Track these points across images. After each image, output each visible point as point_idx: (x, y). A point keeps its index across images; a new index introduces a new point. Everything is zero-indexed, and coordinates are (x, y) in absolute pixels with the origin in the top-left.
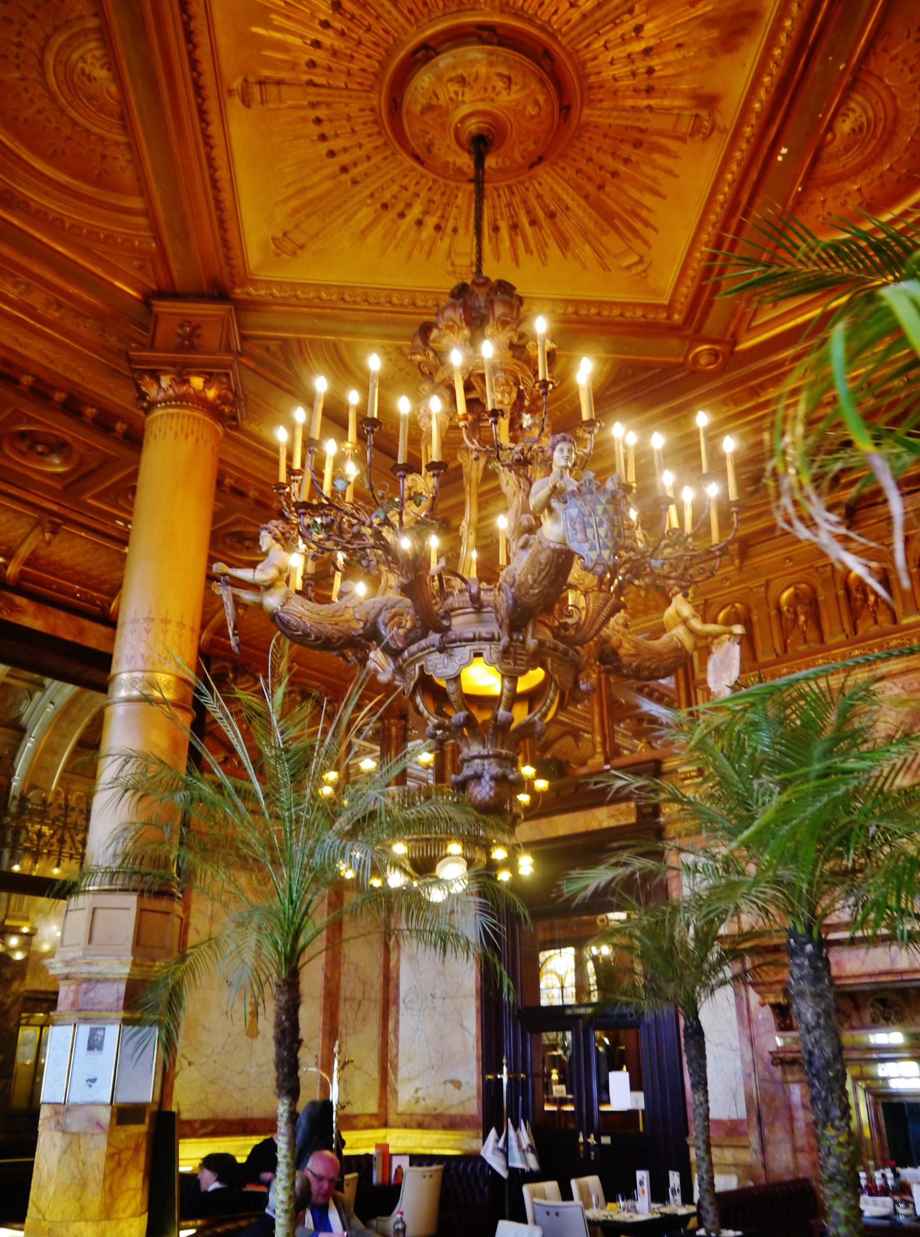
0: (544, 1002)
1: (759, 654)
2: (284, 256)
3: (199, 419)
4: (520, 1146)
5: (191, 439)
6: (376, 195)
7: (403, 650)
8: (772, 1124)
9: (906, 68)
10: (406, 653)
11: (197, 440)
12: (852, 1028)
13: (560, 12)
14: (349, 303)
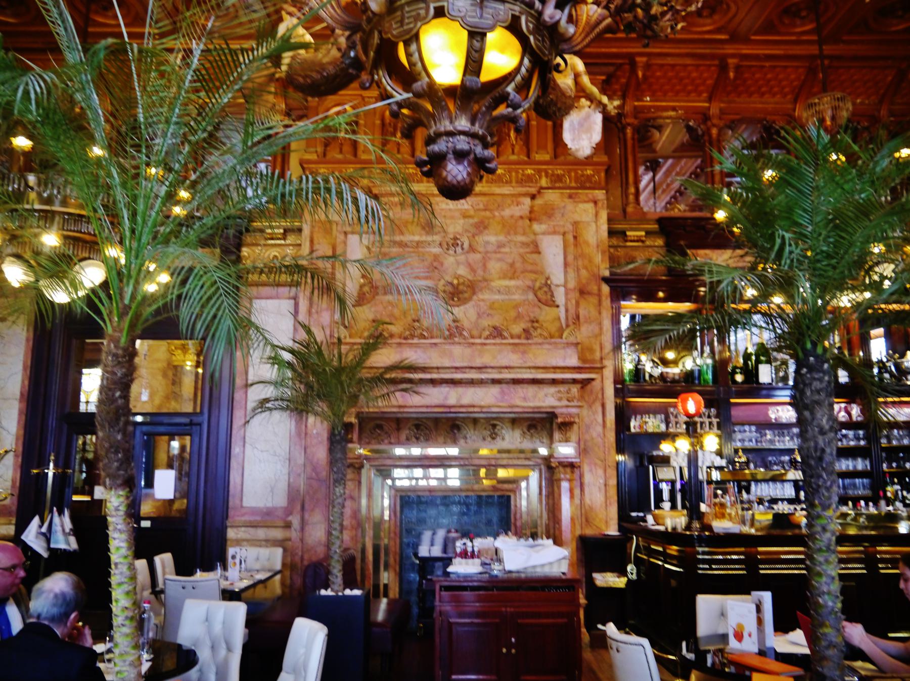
0: (83, 408)
4: (64, 530)
8: (312, 510)
12: (390, 443)
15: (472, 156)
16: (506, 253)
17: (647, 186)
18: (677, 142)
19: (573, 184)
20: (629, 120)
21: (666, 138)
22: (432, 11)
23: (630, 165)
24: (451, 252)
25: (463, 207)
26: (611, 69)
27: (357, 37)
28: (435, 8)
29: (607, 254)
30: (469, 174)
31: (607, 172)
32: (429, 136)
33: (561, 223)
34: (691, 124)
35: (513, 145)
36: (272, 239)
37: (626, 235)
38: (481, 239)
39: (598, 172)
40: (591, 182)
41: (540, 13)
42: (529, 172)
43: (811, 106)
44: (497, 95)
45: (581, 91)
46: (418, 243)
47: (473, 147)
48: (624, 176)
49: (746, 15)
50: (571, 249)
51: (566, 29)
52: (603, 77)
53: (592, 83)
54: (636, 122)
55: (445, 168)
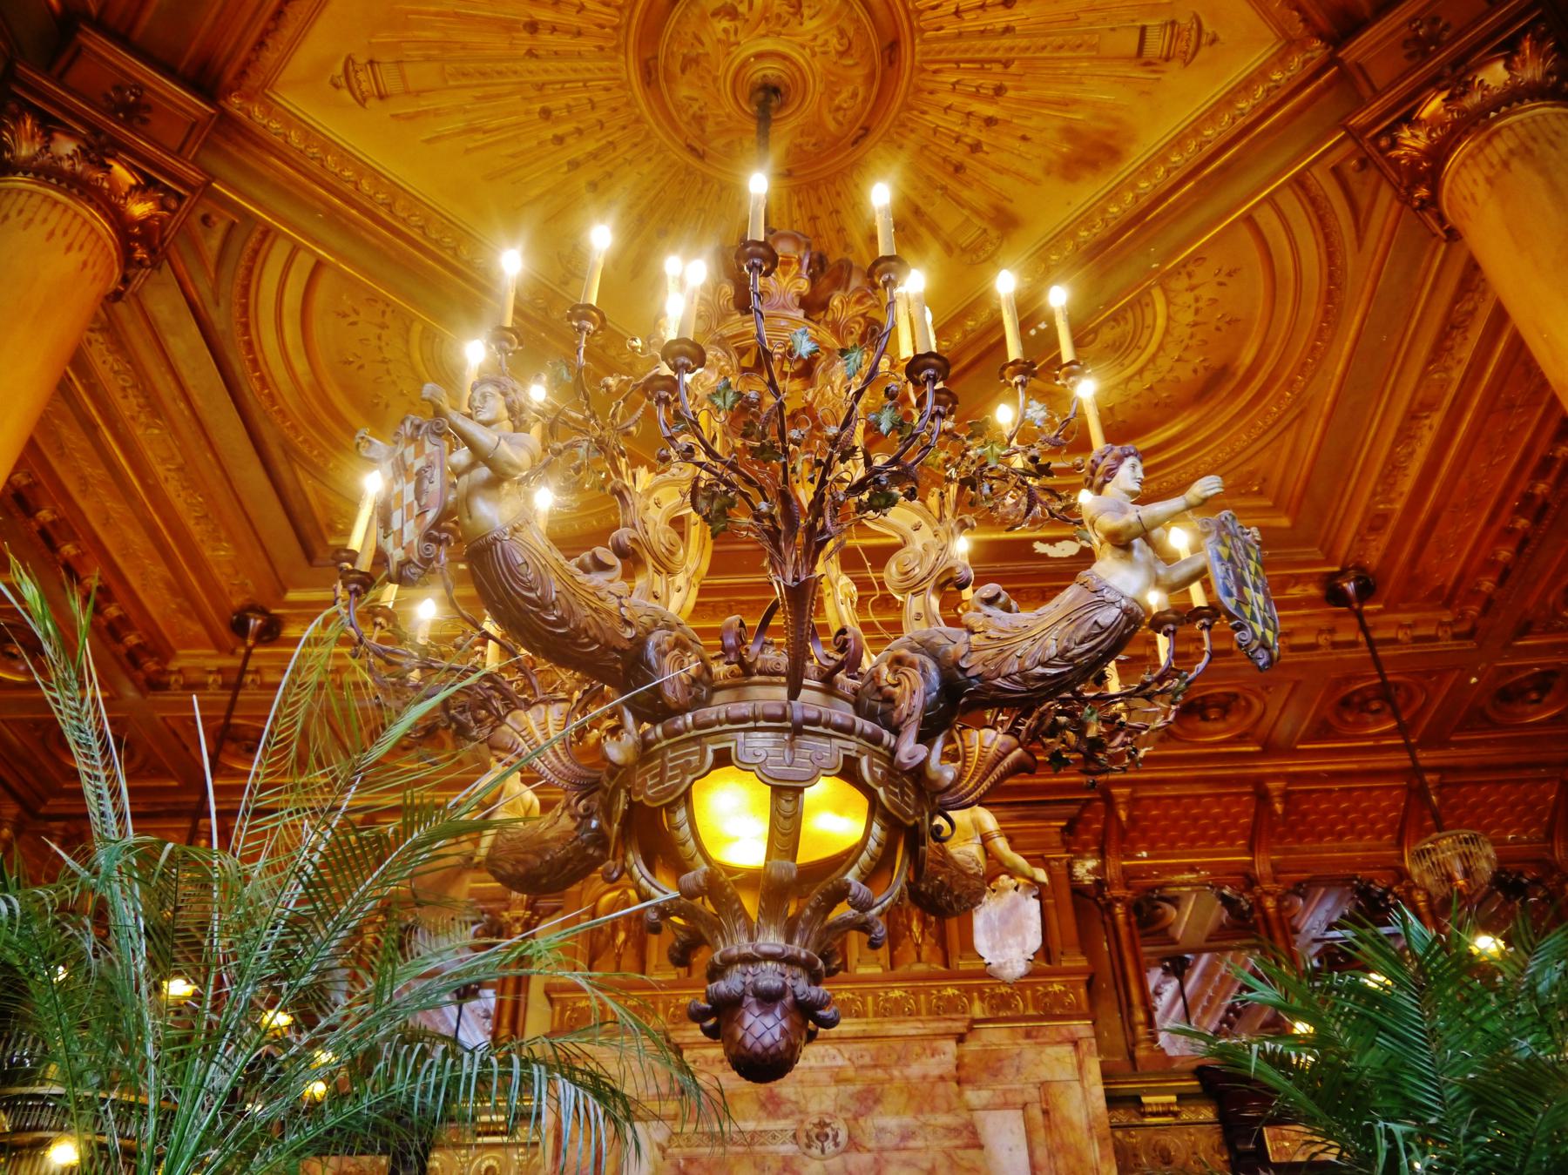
1: (650, 967)
2: (346, 93)
3: (99, 237)
5: (76, 257)
6: (549, 90)
7: (682, 711)
9: (1194, 306)
10: (689, 717)
11: (85, 264)
13: (939, 12)
15: (789, 999)
16: (918, 1150)
17: (1173, 1003)
19: (1031, 1012)
21: (1190, 916)
22: (710, 757)
24: (815, 1151)
25: (834, 1063)
26: (1074, 809)
28: (715, 751)
29: (1110, 1142)
30: (784, 1032)
31: (1089, 985)
32: (713, 964)
33: (1017, 1086)
34: (1226, 891)
35: (917, 945)
36: (487, 1134)
37: (1142, 1105)
39: (1074, 987)
40: (1063, 1006)
41: (894, 751)
42: (950, 991)
43: (1422, 854)
46: (754, 1134)
47: (789, 982)
50: (1040, 1136)
51: (940, 773)
52: (1063, 824)
53: (1013, 849)
54: (1129, 894)
55: (740, 1021)
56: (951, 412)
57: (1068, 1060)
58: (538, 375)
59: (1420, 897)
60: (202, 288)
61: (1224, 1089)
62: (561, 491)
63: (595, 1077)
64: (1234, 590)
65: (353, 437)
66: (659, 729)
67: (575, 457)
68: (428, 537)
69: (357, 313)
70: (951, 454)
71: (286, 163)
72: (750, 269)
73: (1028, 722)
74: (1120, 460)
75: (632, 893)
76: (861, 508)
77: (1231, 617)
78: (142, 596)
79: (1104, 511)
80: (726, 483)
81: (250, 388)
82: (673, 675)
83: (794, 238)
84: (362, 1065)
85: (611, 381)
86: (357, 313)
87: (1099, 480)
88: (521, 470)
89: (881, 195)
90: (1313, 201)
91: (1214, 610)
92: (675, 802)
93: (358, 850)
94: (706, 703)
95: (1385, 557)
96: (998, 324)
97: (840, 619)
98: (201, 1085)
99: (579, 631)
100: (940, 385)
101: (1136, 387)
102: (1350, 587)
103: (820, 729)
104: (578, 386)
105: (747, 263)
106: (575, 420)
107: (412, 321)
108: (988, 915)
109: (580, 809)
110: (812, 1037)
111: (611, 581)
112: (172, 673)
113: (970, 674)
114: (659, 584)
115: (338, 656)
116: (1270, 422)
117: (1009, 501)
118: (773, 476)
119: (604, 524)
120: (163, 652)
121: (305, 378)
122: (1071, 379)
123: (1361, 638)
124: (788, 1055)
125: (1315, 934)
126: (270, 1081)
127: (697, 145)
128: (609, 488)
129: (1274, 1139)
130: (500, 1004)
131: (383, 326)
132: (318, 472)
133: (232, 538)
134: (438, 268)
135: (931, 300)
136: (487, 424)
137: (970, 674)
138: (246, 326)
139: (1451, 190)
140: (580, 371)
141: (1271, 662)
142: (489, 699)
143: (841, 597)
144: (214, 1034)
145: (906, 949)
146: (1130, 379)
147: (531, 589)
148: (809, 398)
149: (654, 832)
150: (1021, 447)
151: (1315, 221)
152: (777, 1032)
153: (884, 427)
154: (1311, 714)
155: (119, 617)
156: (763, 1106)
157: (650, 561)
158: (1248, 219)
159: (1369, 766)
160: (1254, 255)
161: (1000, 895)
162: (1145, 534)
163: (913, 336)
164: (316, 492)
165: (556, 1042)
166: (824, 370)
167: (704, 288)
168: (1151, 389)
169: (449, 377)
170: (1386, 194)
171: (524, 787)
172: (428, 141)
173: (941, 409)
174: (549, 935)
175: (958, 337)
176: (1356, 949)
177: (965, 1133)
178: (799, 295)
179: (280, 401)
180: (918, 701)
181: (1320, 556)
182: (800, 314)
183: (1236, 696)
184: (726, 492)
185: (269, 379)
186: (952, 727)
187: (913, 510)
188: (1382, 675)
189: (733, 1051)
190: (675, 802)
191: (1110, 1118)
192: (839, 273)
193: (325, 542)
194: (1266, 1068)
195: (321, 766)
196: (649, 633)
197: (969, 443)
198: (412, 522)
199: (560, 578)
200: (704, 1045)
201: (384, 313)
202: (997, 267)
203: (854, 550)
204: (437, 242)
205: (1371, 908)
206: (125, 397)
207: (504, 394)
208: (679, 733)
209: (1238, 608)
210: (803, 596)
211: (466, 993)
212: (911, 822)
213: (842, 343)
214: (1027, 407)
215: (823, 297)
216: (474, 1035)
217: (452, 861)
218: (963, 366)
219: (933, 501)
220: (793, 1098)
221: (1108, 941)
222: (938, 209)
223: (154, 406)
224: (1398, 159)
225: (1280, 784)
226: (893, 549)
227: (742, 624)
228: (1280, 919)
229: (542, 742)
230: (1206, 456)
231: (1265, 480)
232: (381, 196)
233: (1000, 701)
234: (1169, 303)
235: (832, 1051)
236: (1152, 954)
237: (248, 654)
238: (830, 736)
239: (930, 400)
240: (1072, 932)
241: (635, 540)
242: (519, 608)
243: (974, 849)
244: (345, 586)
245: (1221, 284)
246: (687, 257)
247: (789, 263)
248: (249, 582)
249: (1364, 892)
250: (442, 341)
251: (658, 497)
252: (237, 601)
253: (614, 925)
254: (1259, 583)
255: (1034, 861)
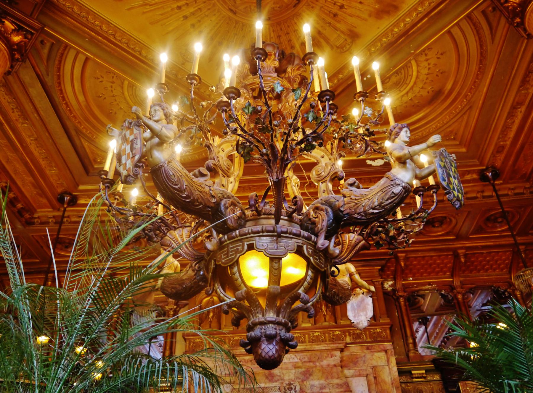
1: (223, 326)
7: (235, 229)
9: (428, 67)
10: (237, 232)
14: (116, 40)
15: (278, 338)
17: (423, 335)
18: (437, 305)
19: (369, 340)
20: (401, 293)
21: (429, 302)
22: (246, 247)
23: (407, 323)
25: (294, 361)
26: (383, 262)
27: (202, 264)
28: (248, 245)
29: (400, 388)
30: (277, 351)
31: (391, 329)
33: (364, 368)
34: (443, 292)
35: (324, 315)
37: (412, 374)
38: (308, 383)
39: (385, 330)
40: (381, 337)
41: (316, 243)
42: (337, 333)
43: (518, 277)
44: (293, 295)
45: (355, 285)
47: (278, 332)
48: (403, 331)
49: (463, 223)
50: (373, 387)
51: (334, 251)
52: (379, 268)
54: (405, 294)
55: (260, 346)
56: (335, 113)
57: (383, 358)
58: (176, 102)
59: (518, 293)
60: (42, 69)
61: (447, 370)
62: (185, 146)
63: (205, 369)
64: (446, 179)
65: (105, 128)
66: (226, 237)
67: (191, 133)
68: (136, 166)
69: (103, 78)
70: (335, 128)
71: (73, 19)
72: (257, 59)
73: (367, 230)
74: (401, 129)
75: (215, 298)
76: (302, 150)
77: (444, 189)
78: (23, 189)
79: (395, 149)
80: (250, 142)
81: (62, 107)
82: (231, 216)
83: (272, 45)
84: (116, 367)
85: (204, 103)
86: (103, 78)
87: (393, 137)
88: (170, 139)
89: (307, 28)
90: (474, 24)
91: (438, 185)
92: (233, 264)
93: (111, 285)
94: (243, 226)
95: (503, 163)
96: (353, 75)
97: (294, 193)
98: (55, 377)
99: (194, 200)
100: (331, 102)
101: (405, 99)
102: (490, 175)
103: (288, 235)
104: (191, 106)
105: (255, 57)
106: (191, 119)
107: (124, 80)
108: (352, 304)
109: (196, 267)
110: (287, 352)
111: (206, 181)
112: (35, 218)
113: (344, 213)
114: (224, 181)
115: (103, 210)
116: (458, 111)
117: (358, 146)
118: (268, 139)
119: (201, 157)
120: (32, 211)
121: (83, 104)
122: (382, 98)
123: (494, 194)
124: (278, 359)
125: (477, 308)
126: (81, 374)
127: (233, 8)
128: (204, 144)
129: (463, 386)
130: (166, 342)
131: (113, 82)
132: (92, 141)
133: (57, 166)
134: (139, 62)
135: (326, 69)
136: (157, 121)
137: (344, 213)
138: (60, 84)
139: (529, 19)
140: (192, 100)
141: (461, 206)
142: (160, 226)
143: (293, 184)
144: (59, 357)
145: (320, 317)
146: (403, 96)
147: (176, 185)
148: (280, 107)
149: (225, 275)
150: (362, 125)
151: (475, 33)
152: (274, 350)
153: (310, 119)
154: (475, 224)
155: (14, 197)
156: (267, 378)
157: (220, 172)
158: (449, 32)
159: (498, 243)
160: (452, 46)
161: (357, 296)
162: (411, 157)
163: (320, 82)
164: (89, 147)
165: (190, 356)
166: (285, 97)
167: (239, 66)
168: (411, 99)
169: (141, 103)
170: (503, 21)
171: (174, 260)
172: (129, 9)
173: (332, 111)
174: (184, 315)
175: (336, 81)
176: (493, 313)
177: (344, 386)
178: (275, 67)
179: (74, 113)
180: (325, 224)
181: (478, 163)
182: (276, 75)
183: (445, 217)
184: (250, 146)
185: (69, 104)
186: (338, 233)
187: (321, 150)
188: (502, 208)
189: (257, 358)
190: (233, 264)
191: (400, 379)
192: (290, 58)
193: (93, 167)
194: (461, 361)
195: (97, 254)
196: (221, 200)
197: (342, 124)
198: (130, 160)
199: (187, 180)
200: (244, 355)
201: (113, 77)
202: (351, 54)
203: (298, 165)
204: (133, 49)
205: (499, 297)
206: (13, 112)
207: (163, 110)
208: (234, 238)
209: (448, 185)
210: (280, 184)
211: (152, 338)
212: (323, 270)
213: (292, 86)
214: (364, 109)
215: (284, 68)
216: (156, 354)
217: (147, 289)
218: (340, 93)
219: (329, 147)
220: (279, 374)
221: (397, 313)
222: (327, 31)
223: (25, 115)
224: (508, 7)
225: (463, 251)
226: (314, 164)
227: (256, 196)
228: (464, 302)
229: (181, 243)
230: (433, 125)
231: (456, 134)
232: (97, 23)
233: (355, 222)
234: (418, 66)
235: (293, 356)
236: (414, 316)
237: (65, 210)
238: (291, 238)
239: (327, 108)
240: (384, 309)
241: (214, 164)
242: (171, 192)
243: (347, 279)
244: (103, 185)
245: (438, 58)
246: (231, 55)
247: (271, 55)
248: (64, 183)
249: (496, 292)
250: (136, 87)
251: (223, 147)
252: (60, 190)
253: (209, 312)
254: (456, 176)
255: (370, 283)
